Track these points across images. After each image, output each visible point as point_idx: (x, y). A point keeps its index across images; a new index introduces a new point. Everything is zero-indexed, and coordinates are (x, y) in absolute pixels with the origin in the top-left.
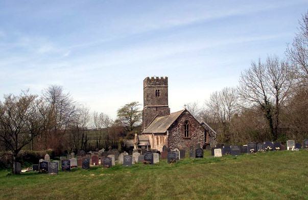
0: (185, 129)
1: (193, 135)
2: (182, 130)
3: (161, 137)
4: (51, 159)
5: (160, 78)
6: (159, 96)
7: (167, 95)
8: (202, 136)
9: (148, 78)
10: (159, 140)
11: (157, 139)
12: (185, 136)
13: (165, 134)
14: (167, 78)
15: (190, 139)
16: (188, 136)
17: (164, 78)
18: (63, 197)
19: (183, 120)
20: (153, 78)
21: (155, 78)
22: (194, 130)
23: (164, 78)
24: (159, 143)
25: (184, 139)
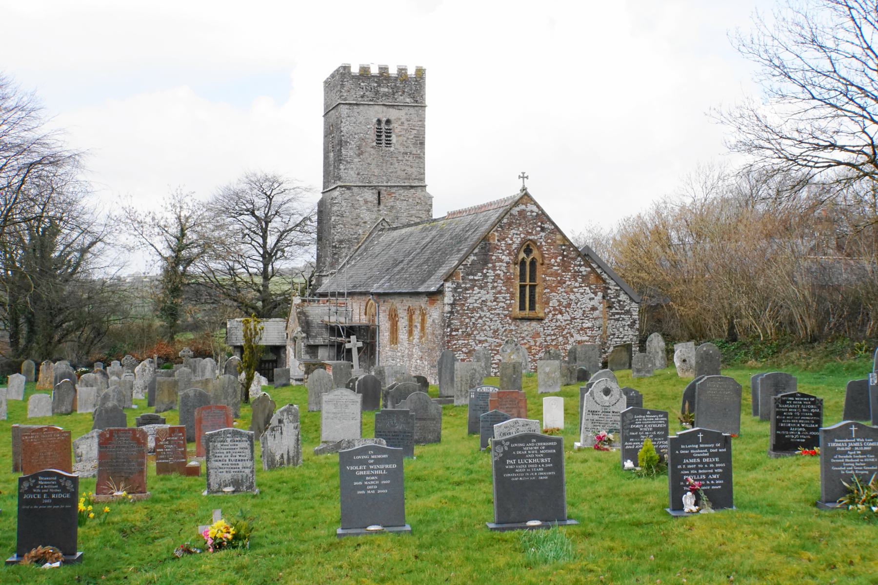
0: (522, 277)
1: (553, 303)
2: (508, 281)
3: (411, 312)
4: (731, 506)
5: (374, 71)
6: (389, 144)
7: (325, 136)
8: (594, 309)
9: (346, 68)
10: (403, 323)
11: (393, 317)
12: (522, 307)
13: (435, 295)
14: (421, 73)
15: (540, 320)
16: (532, 308)
17: (411, 72)
18: (217, 568)
19: (516, 237)
20: (384, 70)
21: (374, 71)
22: (561, 283)
23: (411, 72)
24: (403, 335)
25: (515, 319)
